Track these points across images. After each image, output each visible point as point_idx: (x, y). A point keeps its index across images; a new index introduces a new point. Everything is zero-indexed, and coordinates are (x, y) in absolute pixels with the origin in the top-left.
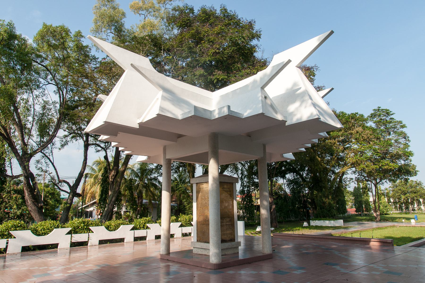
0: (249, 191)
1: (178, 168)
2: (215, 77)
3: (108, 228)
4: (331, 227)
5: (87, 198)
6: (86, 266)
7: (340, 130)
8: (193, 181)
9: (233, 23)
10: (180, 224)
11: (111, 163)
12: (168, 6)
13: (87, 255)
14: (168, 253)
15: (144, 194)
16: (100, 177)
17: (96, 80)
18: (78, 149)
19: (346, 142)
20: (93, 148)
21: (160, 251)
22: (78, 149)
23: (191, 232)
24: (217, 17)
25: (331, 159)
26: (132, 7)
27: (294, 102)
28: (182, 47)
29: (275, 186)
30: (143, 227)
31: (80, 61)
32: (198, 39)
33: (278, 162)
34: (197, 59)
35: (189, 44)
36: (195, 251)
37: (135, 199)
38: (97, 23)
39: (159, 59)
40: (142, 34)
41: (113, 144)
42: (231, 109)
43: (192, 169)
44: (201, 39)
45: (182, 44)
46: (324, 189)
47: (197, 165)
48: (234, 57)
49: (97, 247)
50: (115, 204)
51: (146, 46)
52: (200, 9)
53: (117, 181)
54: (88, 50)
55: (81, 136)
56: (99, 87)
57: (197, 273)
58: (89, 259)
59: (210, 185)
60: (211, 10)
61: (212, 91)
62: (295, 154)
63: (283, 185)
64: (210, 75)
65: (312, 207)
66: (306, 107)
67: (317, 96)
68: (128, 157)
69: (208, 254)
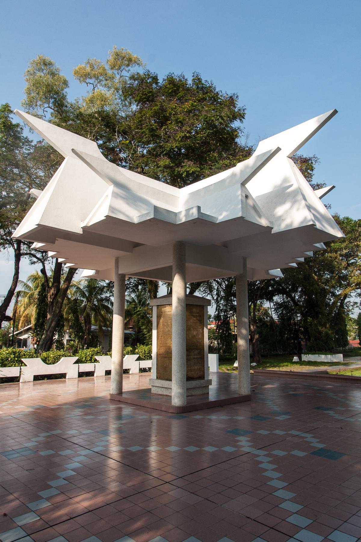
0: (226, 317)
1: (136, 286)
2: (183, 169)
3: (45, 360)
4: (328, 363)
5: (21, 322)
6: (16, 407)
7: (342, 240)
8: (152, 303)
9: (209, 97)
10: (137, 356)
11: (50, 278)
12: (124, 73)
13: (19, 394)
14: (120, 391)
15: (93, 319)
16: (36, 296)
17: (30, 170)
18: (8, 259)
19: (351, 256)
20: (27, 258)
21: (110, 391)
22: (8, 259)
23: (150, 366)
24: (188, 89)
25: (331, 277)
26: (76, 73)
27: (283, 202)
28: (141, 129)
29: (259, 311)
30: (91, 360)
31: (9, 145)
32: (163, 119)
33: (264, 280)
34: (161, 144)
35: (151, 125)
36: (154, 390)
37: (80, 324)
38: (30, 94)
39: (112, 145)
40: (89, 110)
41: (50, 254)
42: (202, 211)
43: (153, 288)
44: (167, 119)
45: (141, 125)
46: (320, 316)
47: (160, 283)
48: (209, 143)
49: (32, 384)
50: (56, 331)
51: (94, 126)
52: (166, 78)
53: (58, 302)
54: (19, 129)
55: (11, 242)
56: (33, 180)
57: (155, 418)
58: (20, 398)
59: (174, 308)
60: (180, 80)
61: (180, 187)
62: (284, 271)
63: (270, 310)
64: (178, 167)
65: (305, 338)
66: (298, 209)
67: (313, 196)
68: (72, 271)
69: (170, 395)
